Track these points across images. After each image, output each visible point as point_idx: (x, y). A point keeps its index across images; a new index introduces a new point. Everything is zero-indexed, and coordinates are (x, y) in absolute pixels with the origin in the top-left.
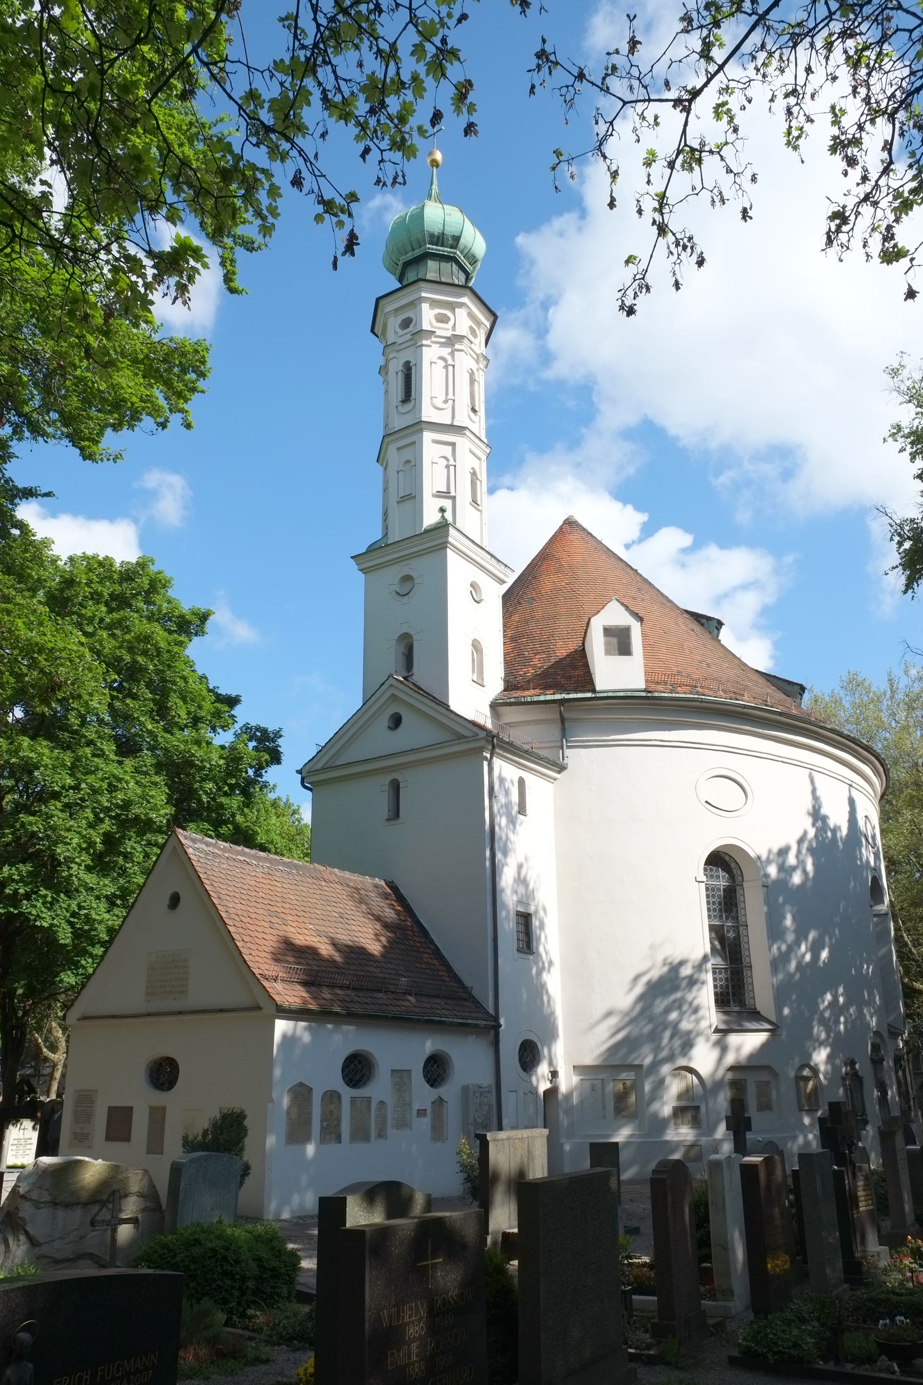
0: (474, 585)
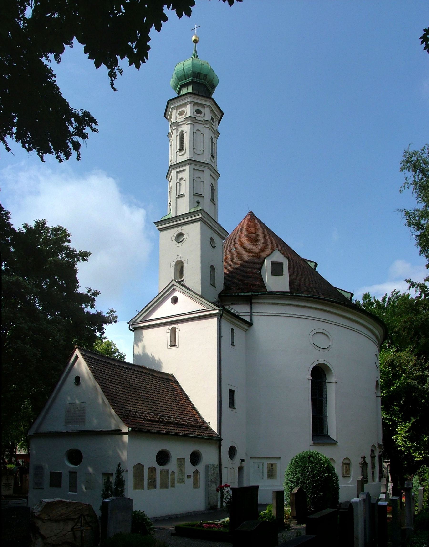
0: (212, 239)
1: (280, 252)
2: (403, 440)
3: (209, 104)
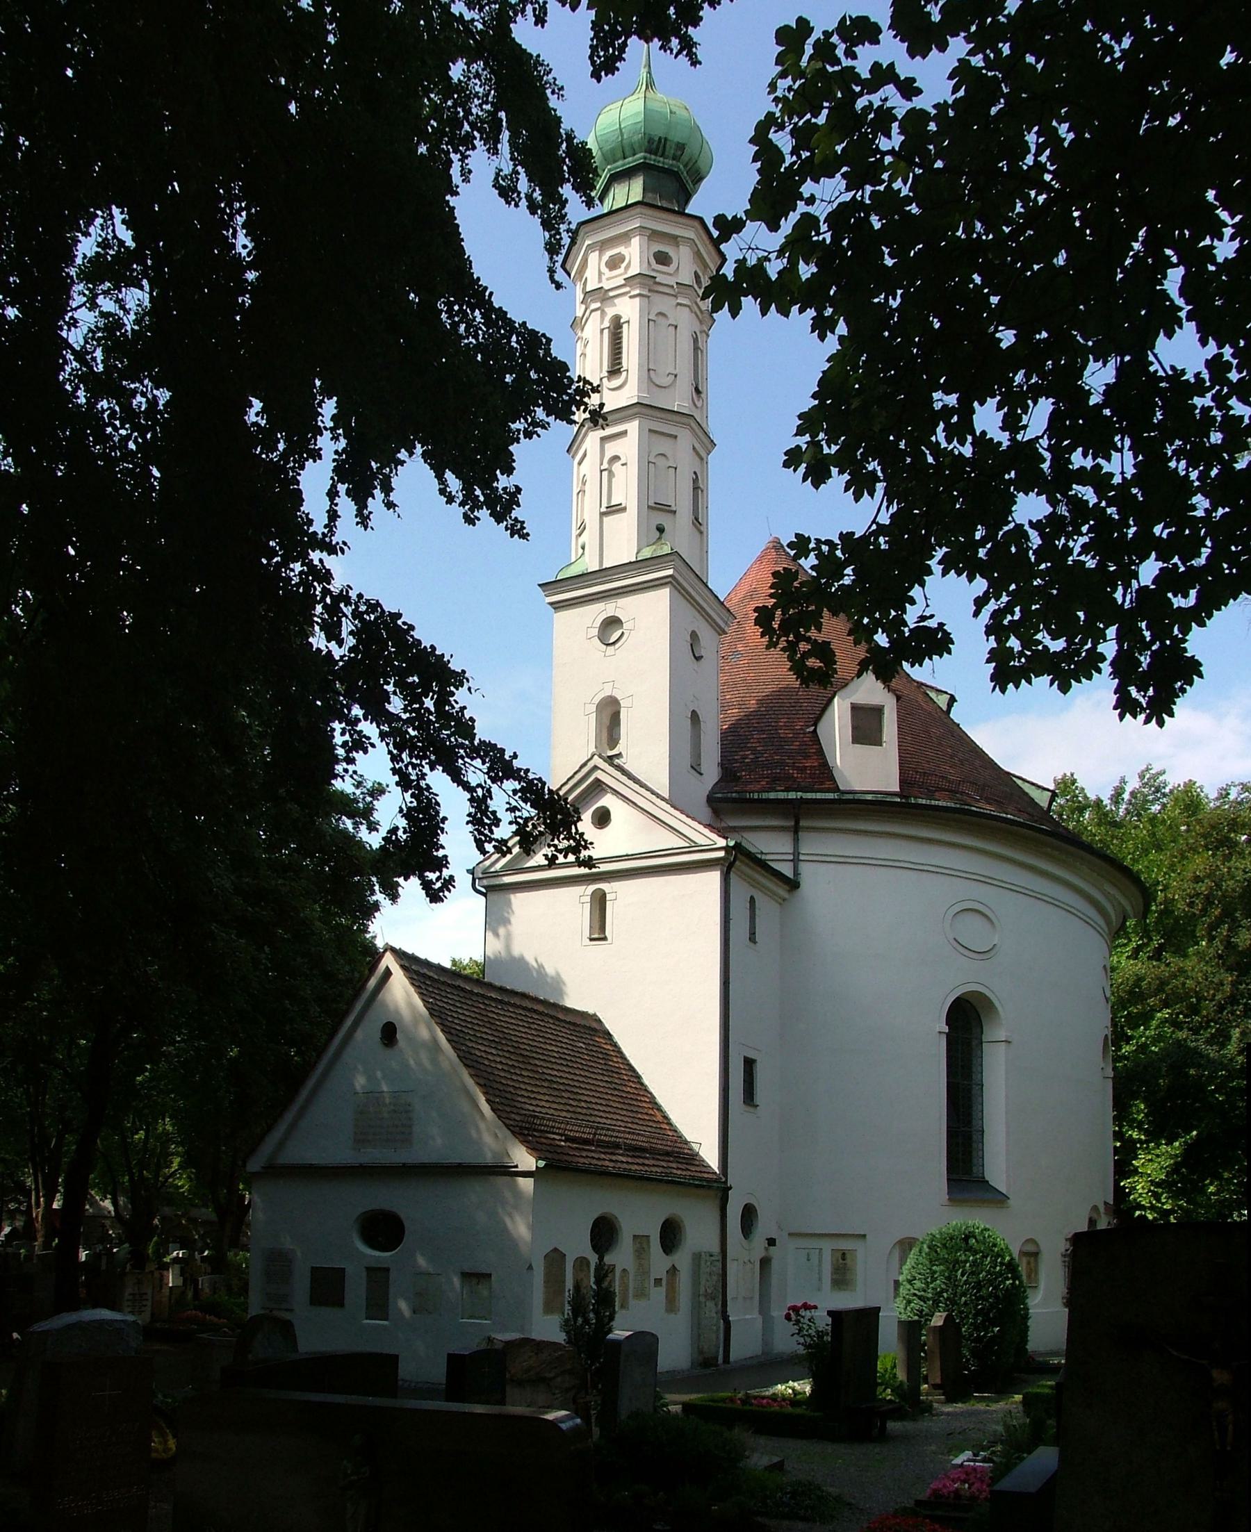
0: (694, 636)
2: (1150, 1191)
3: (690, 234)
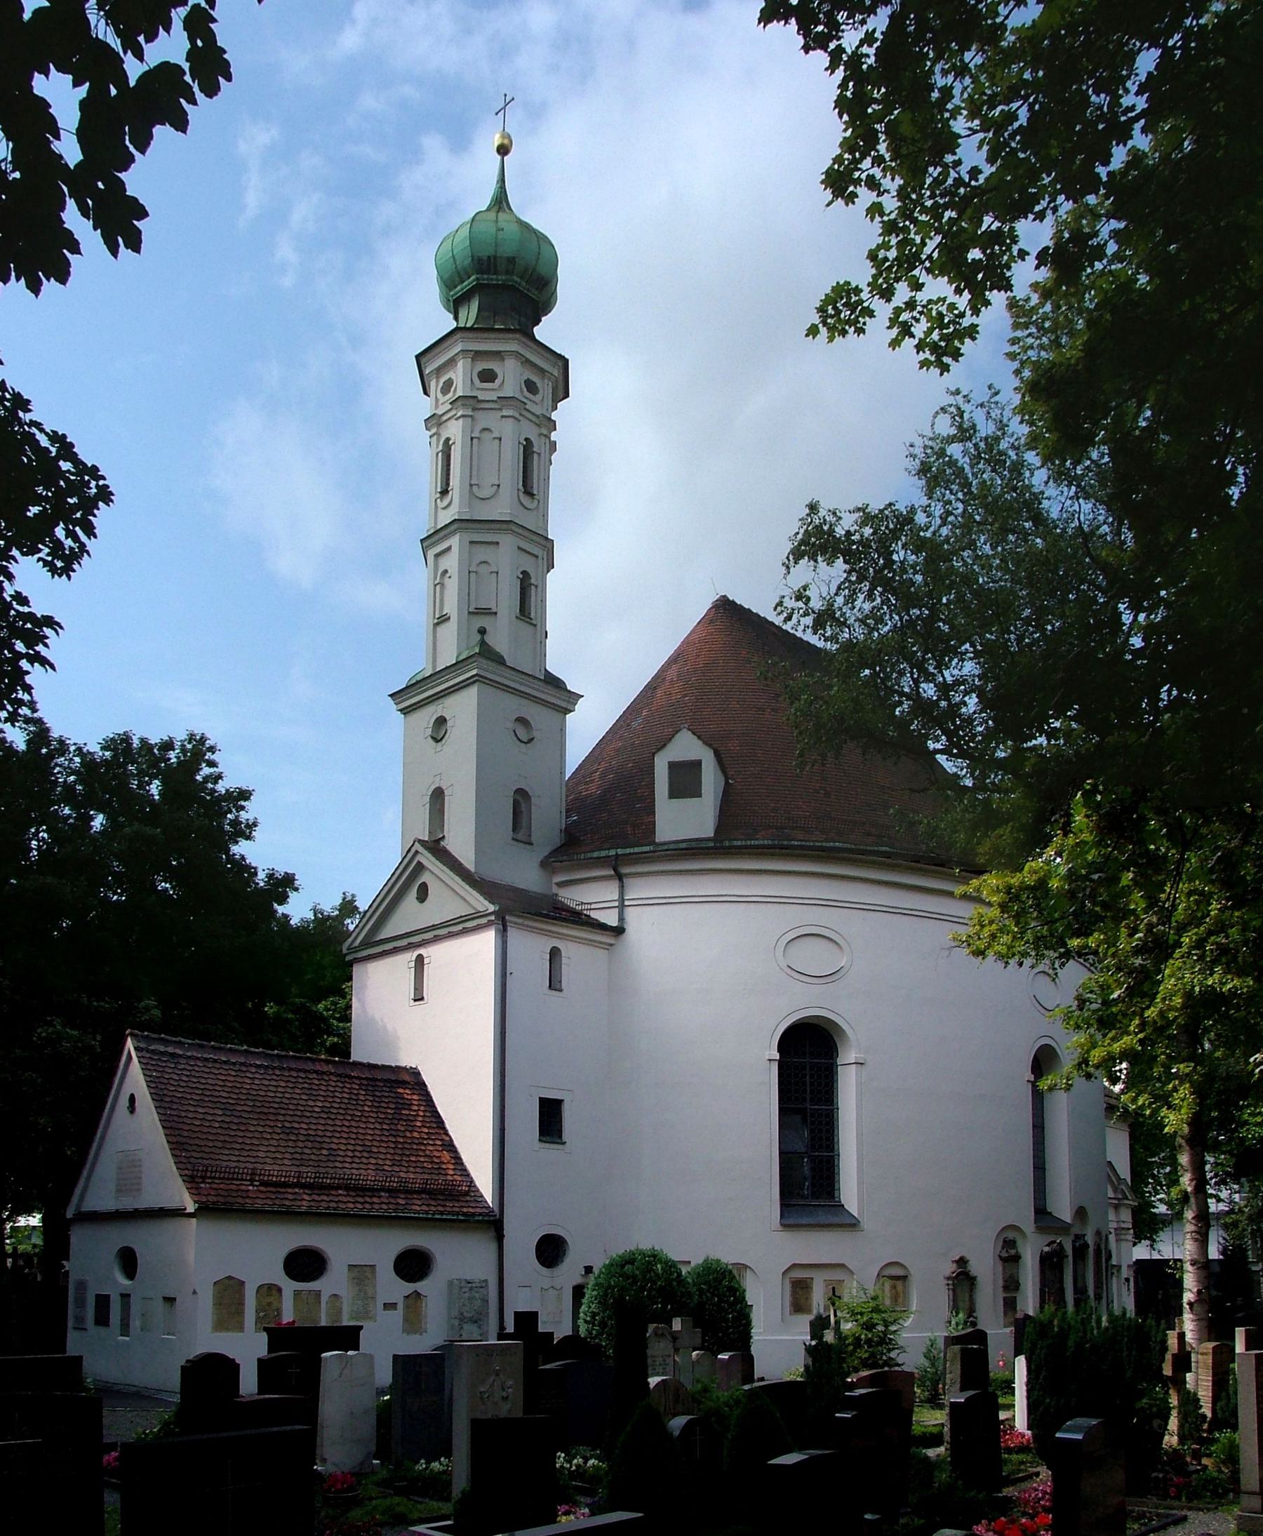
1: (694, 733)
